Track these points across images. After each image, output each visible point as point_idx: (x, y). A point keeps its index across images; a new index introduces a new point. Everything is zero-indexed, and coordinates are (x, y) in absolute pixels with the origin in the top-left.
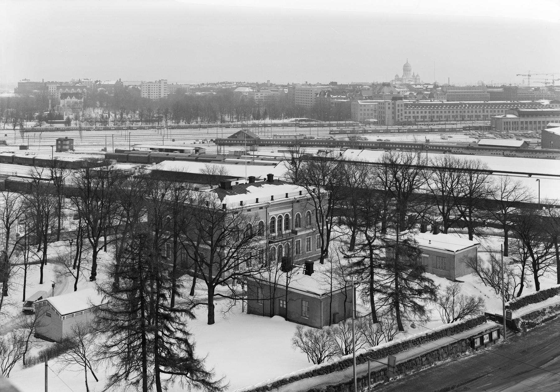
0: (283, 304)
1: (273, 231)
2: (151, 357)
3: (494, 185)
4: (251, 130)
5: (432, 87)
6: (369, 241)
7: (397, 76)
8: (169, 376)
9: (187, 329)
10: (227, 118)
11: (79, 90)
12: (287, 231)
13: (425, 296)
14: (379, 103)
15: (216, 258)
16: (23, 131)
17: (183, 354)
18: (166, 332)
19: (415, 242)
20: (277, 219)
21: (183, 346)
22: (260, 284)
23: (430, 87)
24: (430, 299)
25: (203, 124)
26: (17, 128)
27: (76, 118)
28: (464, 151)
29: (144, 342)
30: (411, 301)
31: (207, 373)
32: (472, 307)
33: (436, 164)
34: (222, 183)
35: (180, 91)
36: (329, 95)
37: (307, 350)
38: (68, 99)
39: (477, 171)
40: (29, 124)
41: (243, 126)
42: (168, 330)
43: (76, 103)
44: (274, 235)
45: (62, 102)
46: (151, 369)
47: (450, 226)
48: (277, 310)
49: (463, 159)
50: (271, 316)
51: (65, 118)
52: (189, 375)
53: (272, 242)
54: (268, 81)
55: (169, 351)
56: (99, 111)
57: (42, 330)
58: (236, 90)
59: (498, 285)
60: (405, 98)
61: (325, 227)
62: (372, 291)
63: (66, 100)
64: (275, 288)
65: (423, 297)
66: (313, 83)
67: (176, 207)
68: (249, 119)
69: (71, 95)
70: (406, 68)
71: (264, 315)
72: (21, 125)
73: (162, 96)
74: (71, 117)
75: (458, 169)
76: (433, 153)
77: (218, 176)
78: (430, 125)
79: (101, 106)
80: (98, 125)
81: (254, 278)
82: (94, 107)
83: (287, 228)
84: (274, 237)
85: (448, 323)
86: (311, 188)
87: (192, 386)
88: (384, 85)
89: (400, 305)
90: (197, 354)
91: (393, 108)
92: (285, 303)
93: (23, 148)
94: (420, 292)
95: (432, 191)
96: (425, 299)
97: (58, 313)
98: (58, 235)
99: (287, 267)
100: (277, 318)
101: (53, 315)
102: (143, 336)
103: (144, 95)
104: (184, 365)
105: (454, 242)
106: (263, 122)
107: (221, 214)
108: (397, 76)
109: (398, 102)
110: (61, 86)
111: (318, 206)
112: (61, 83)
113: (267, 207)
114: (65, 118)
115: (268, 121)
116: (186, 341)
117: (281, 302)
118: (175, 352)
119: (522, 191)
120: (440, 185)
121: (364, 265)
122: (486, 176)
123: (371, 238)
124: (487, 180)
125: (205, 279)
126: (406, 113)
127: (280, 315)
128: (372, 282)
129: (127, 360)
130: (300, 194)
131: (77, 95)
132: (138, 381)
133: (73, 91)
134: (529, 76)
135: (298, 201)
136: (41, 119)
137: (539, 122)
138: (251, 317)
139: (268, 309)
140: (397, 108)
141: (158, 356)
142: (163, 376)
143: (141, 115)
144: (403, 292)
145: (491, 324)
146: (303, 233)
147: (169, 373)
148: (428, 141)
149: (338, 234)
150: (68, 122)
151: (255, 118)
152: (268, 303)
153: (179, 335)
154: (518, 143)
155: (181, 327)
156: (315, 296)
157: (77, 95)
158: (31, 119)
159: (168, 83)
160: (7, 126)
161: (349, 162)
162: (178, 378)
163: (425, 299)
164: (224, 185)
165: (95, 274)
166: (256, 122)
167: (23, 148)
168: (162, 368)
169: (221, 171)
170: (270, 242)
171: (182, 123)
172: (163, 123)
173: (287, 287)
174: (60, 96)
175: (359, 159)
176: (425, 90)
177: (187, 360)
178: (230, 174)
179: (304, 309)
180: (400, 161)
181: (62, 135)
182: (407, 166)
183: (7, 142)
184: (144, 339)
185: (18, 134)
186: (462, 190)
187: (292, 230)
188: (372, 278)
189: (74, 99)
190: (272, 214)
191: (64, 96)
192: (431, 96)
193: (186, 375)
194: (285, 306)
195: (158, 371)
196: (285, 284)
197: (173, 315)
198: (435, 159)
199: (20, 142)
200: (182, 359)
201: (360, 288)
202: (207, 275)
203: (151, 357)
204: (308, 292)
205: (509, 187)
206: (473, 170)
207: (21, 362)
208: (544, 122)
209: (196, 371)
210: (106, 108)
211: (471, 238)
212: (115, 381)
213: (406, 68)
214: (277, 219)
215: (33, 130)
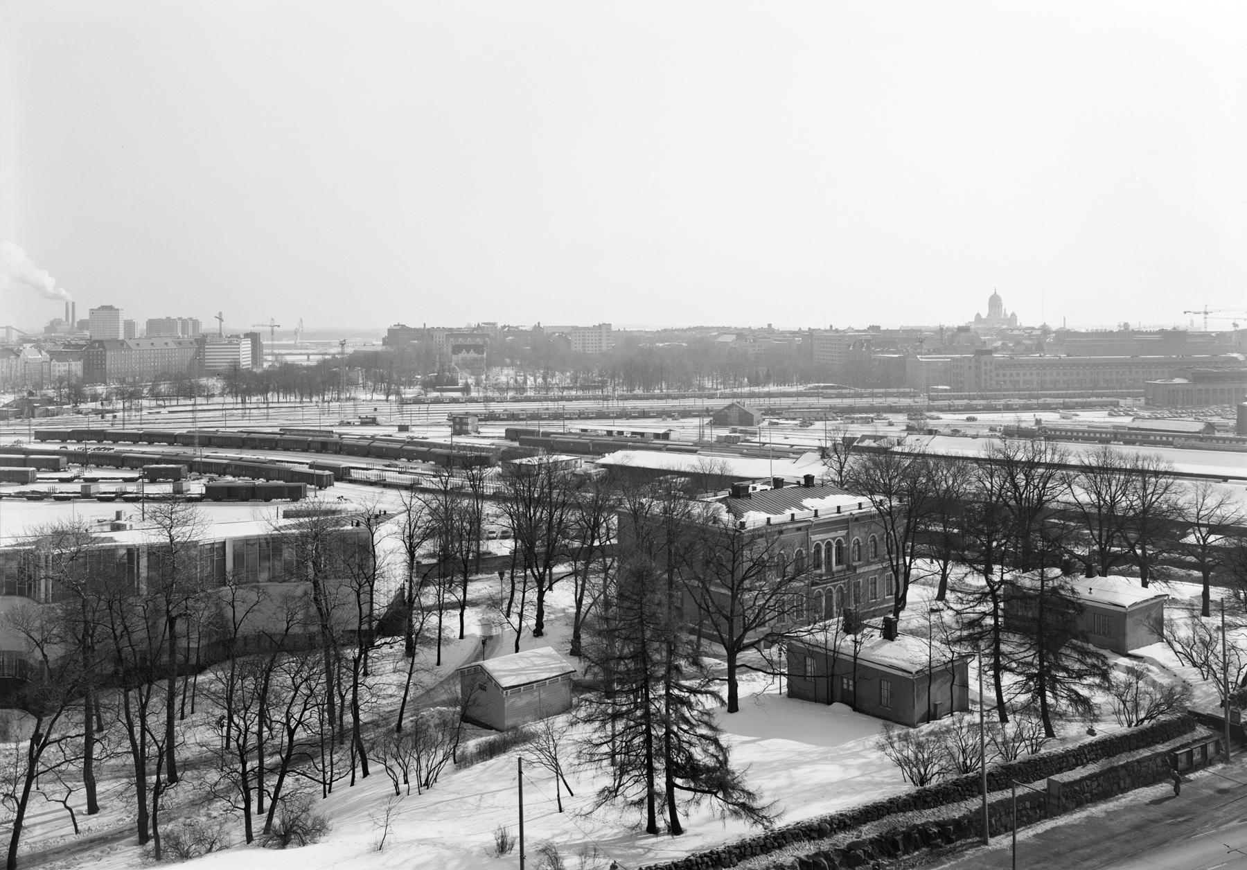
0: (848, 684)
1: (818, 566)
2: (659, 765)
3: (1185, 497)
4: (747, 401)
5: (1039, 332)
6: (991, 587)
7: (978, 315)
8: (690, 795)
9: (715, 723)
10: (708, 384)
11: (479, 341)
12: (840, 567)
13: (1089, 680)
14: (953, 359)
15: (738, 608)
16: (403, 402)
17: (711, 762)
18: (685, 727)
19: (1073, 590)
20: (823, 547)
21: (712, 749)
22: (811, 651)
23: (1035, 333)
24: (1099, 686)
25: (671, 392)
26: (392, 398)
27: (477, 384)
28: (1198, 443)
29: (648, 741)
30: (1070, 690)
31: (749, 794)
32: (1170, 698)
33: (1087, 462)
34: (733, 487)
35: (630, 339)
36: (868, 347)
37: (902, 763)
38: (464, 354)
39: (1156, 474)
40: (410, 393)
41: (734, 396)
42: (687, 721)
43: (475, 359)
44: (818, 572)
45: (454, 357)
46: (660, 783)
47: (1111, 564)
48: (838, 692)
49: (1125, 454)
50: (829, 703)
51: (461, 382)
52: (720, 795)
53: (817, 584)
54: (770, 325)
55: (690, 757)
56: (510, 372)
57: (473, 712)
58: (719, 340)
59: (1206, 663)
60: (996, 350)
61: (901, 562)
62: (998, 669)
63: (461, 356)
64: (835, 660)
65: (1085, 682)
66: (841, 328)
67: (672, 527)
68: (741, 385)
69: (468, 348)
70: (995, 302)
71: (816, 700)
72: (398, 393)
73: (604, 348)
74: (470, 381)
75: (1126, 470)
76: (1078, 441)
77: (717, 475)
78: (493, 400)
79: (512, 364)
80: (511, 394)
81: (801, 641)
82: (503, 365)
83: (839, 562)
84: (821, 576)
85: (1129, 726)
86: (878, 498)
87: (727, 813)
88: (960, 329)
89: (1048, 693)
90: (736, 761)
91: (976, 368)
92: (851, 682)
93: (403, 428)
94: (1080, 675)
95: (1079, 504)
96: (1090, 686)
97: (497, 685)
98: (485, 563)
99: (853, 625)
100: (837, 706)
101: (490, 686)
102: (648, 731)
103: (577, 347)
104: (710, 778)
105: (1124, 590)
106: (766, 389)
107: (737, 539)
108: (978, 315)
109: (984, 358)
110: (451, 333)
111: (889, 527)
112: (451, 329)
113: (807, 528)
114: (461, 382)
115: (772, 388)
116: (716, 742)
117: (845, 681)
118: (699, 757)
119: (1233, 508)
120: (1094, 496)
121: (981, 626)
122: (1170, 481)
123: (995, 583)
124: (1172, 488)
125: (723, 642)
126: (998, 375)
127: (843, 701)
128: (997, 653)
129: (622, 770)
130: (860, 508)
131: (478, 349)
132: (641, 801)
133: (469, 341)
134: (1206, 313)
135: (857, 519)
136: (428, 385)
137: (1230, 390)
138: (797, 704)
139: (823, 691)
140: (984, 368)
141: (670, 762)
142: (680, 796)
143: (575, 379)
144: (1053, 672)
145: (1201, 731)
146: (866, 569)
147: (689, 789)
148: (1038, 422)
149: (922, 573)
150: (466, 389)
151: (751, 384)
152: (832, 686)
153: (703, 731)
154: (1194, 426)
155: (706, 718)
156: (906, 674)
157: (478, 349)
158: (411, 384)
159: (614, 329)
160: (376, 397)
161: (935, 456)
162: (707, 800)
163: (1090, 686)
164: (738, 490)
165: (542, 626)
166: (756, 389)
167: (403, 428)
168: (679, 781)
169: (722, 469)
170: (813, 584)
171: (638, 391)
172: (608, 391)
173: (855, 657)
174: (450, 350)
175: (953, 452)
176: (1026, 338)
177: (714, 769)
178: (736, 473)
179: (885, 693)
180: (1021, 456)
181: (458, 409)
182: (1031, 465)
183: (379, 419)
184: (650, 735)
185: (395, 407)
186: (1128, 501)
187: (848, 566)
188: (997, 648)
189: (472, 354)
190: (816, 538)
191: (457, 349)
192: (1040, 347)
193: (715, 794)
194: (851, 688)
195: (670, 785)
196: (852, 653)
197: (693, 699)
198: (1079, 453)
199: (399, 420)
200: (708, 769)
201: (974, 664)
202: (726, 636)
203: (659, 765)
204: (891, 667)
205: (1211, 502)
206: (1148, 471)
207: (451, 761)
208: (1237, 390)
209: (733, 788)
210: (520, 368)
211: (1145, 585)
212: (606, 798)
213: (995, 302)
214: (823, 547)
215: (417, 401)
